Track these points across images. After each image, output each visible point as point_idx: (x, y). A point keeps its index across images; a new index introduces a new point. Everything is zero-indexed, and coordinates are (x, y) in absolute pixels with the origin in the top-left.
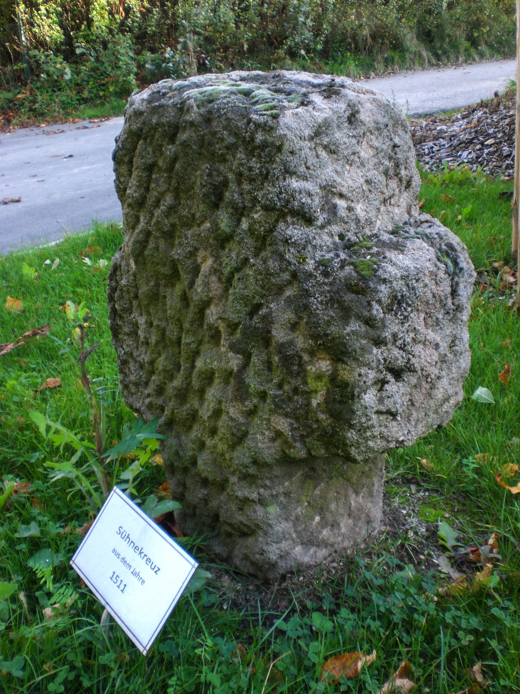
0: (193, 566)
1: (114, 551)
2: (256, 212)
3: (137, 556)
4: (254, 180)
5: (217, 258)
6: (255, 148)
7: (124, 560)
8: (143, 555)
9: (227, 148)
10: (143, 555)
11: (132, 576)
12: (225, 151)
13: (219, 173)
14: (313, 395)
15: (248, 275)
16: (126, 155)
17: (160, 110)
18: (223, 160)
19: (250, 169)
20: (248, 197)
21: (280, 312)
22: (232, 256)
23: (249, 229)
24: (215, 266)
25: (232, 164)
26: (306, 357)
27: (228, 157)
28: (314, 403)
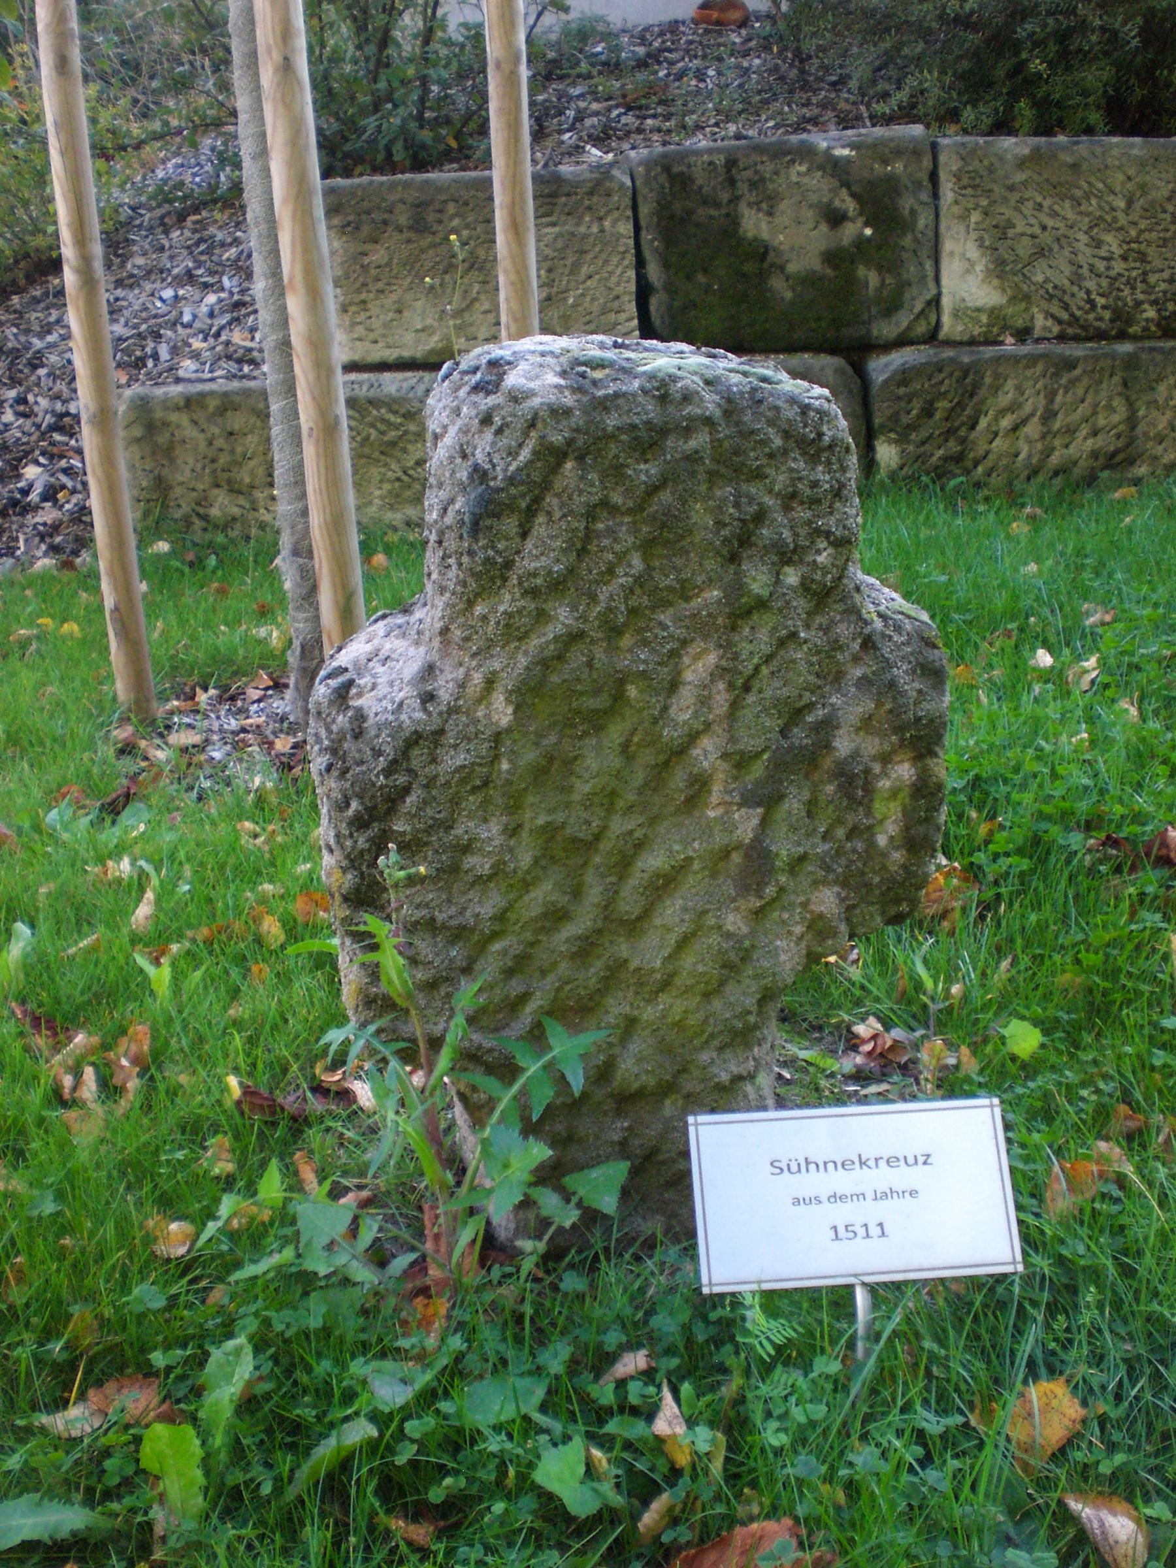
0: (992, 1106)
1: (797, 1202)
2: (819, 552)
3: (858, 1173)
4: (818, 501)
5: (726, 646)
6: (821, 450)
7: (834, 1198)
8: (872, 1163)
9: (771, 456)
10: (872, 1163)
11: (881, 1204)
12: (764, 461)
13: (751, 500)
14: (878, 829)
15: (794, 661)
16: (523, 495)
17: (621, 401)
18: (758, 475)
19: (815, 484)
20: (803, 532)
21: (849, 705)
22: (756, 639)
23: (802, 584)
24: (724, 663)
25: (773, 482)
26: (877, 768)
27: (768, 471)
28: (882, 840)
